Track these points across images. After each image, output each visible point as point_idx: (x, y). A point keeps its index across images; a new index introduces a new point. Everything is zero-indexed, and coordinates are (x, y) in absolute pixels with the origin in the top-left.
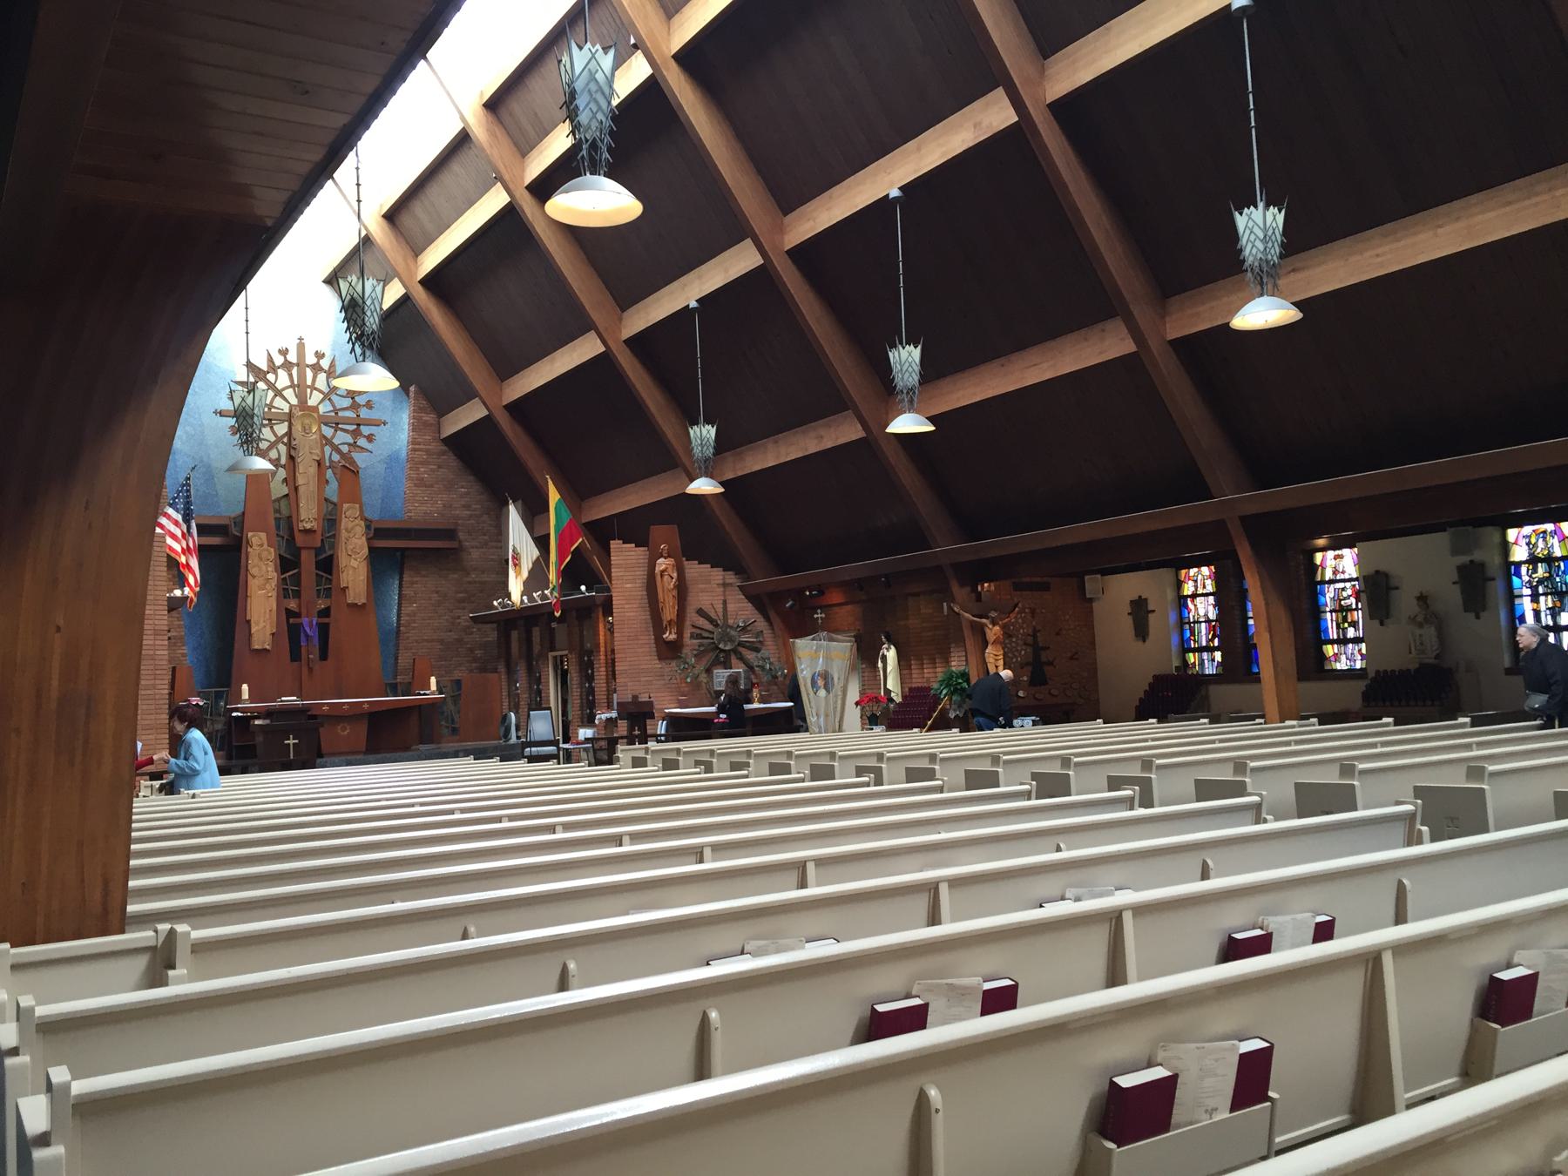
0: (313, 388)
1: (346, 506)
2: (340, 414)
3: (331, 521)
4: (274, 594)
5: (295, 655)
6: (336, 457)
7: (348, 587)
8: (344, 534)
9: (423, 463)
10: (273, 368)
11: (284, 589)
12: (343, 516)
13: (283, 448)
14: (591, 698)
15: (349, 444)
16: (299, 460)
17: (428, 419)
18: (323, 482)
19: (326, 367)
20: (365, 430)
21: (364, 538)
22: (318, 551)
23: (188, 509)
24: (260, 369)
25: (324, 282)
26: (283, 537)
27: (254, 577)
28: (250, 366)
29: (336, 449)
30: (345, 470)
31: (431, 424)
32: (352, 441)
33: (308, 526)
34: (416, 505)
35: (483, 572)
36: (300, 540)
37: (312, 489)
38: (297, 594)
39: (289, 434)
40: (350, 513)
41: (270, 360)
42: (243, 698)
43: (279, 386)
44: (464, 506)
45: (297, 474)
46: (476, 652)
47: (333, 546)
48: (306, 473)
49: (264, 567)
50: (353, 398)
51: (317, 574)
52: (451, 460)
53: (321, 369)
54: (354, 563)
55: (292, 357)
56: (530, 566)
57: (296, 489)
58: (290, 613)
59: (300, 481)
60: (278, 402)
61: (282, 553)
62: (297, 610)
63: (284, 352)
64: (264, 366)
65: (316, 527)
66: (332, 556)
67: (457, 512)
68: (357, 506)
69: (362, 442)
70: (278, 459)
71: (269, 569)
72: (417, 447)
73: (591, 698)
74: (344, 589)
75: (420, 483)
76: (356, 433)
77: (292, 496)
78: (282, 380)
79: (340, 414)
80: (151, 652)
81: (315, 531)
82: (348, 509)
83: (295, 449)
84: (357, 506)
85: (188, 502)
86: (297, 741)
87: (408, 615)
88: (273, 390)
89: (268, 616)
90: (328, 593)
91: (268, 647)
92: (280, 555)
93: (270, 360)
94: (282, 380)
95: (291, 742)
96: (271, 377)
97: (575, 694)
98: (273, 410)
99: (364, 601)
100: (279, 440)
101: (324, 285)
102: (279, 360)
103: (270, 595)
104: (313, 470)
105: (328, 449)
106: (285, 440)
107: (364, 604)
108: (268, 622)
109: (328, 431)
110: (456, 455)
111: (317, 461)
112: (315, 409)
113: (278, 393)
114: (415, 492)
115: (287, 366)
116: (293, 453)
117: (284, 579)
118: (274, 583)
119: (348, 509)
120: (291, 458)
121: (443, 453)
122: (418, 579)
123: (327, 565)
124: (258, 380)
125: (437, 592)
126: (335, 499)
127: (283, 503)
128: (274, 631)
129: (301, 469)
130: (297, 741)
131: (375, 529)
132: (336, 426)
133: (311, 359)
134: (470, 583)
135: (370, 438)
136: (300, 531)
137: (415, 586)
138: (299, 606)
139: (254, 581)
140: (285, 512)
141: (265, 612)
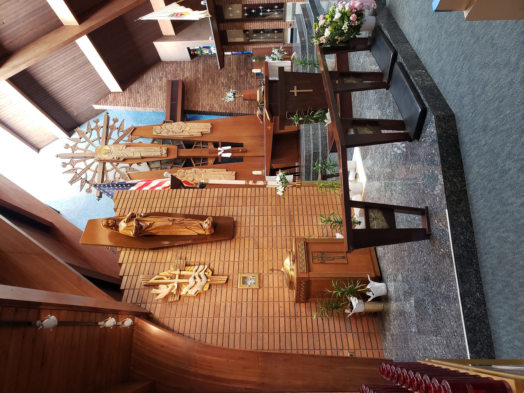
0: (86, 150)
1: (154, 133)
2: (101, 136)
3: (164, 141)
4: (204, 170)
5: (240, 159)
6: (126, 138)
7: (201, 132)
8: (170, 134)
9: (136, 101)
10: (74, 170)
11: (202, 165)
12: (160, 134)
13: (121, 165)
14: (276, 7)
15: (119, 132)
16: (126, 156)
17: (111, 98)
18: (140, 145)
19: (74, 143)
20: (111, 123)
21: (173, 124)
22: (179, 147)
23: (117, 185)
24: (74, 177)
25: (38, 152)
26: (172, 166)
27: (194, 180)
28: (72, 182)
29: (121, 138)
30: (134, 133)
31: (115, 97)
32: (117, 130)
33: (164, 152)
34: (159, 104)
35: (198, 71)
36: (173, 156)
37: (143, 150)
38: (205, 159)
39: (111, 162)
40: (156, 131)
41: (69, 171)
42: (261, 174)
43: (84, 167)
44: (160, 80)
45: (134, 157)
46: (242, 74)
47: (178, 140)
48: (131, 152)
49: (189, 175)
50: (92, 130)
51: (194, 148)
52: (134, 86)
53: (75, 146)
54: (188, 129)
55: (67, 161)
56: (183, 7)
57: (143, 158)
58: (216, 162)
59: (138, 155)
60: (93, 167)
61: (182, 166)
62: (215, 159)
63: (64, 165)
64: (71, 175)
65: (165, 148)
66: (184, 141)
67: (164, 83)
68: (154, 127)
69: (117, 125)
70: (126, 167)
71: (189, 172)
72: (126, 103)
73: (276, 7)
74: (202, 134)
75: (147, 103)
76: (113, 128)
77: (148, 160)
78: (81, 165)
79: (101, 136)
80: (215, 199)
81: (168, 148)
82: (156, 131)
83: (119, 158)
84: (154, 127)
85: (113, 186)
86: (296, 95)
87: (220, 109)
88: (86, 170)
89: (217, 173)
90: (205, 143)
91: (234, 173)
92: (183, 167)
93: (69, 171)
94: (81, 165)
95: (295, 91)
96: (79, 171)
97: (271, 46)
98: (87, 152)
99: (209, 124)
100: (114, 167)
101: (40, 153)
102: (69, 167)
103: (204, 172)
104: (132, 149)
105: (121, 142)
106: (115, 164)
107: (211, 124)
108: (220, 172)
109: (111, 142)
110: (132, 84)
111: (127, 146)
112: (97, 148)
113: (88, 167)
114: (152, 105)
115: (72, 164)
116: (122, 159)
117: (196, 165)
118: (198, 170)
119: (156, 131)
120: (125, 160)
121: (131, 90)
122: (200, 103)
123: (189, 144)
124: (80, 178)
125: (208, 94)
126: (151, 140)
127: (152, 166)
128: (225, 170)
129: (131, 155)
130: (296, 95)
131: (171, 119)
132: (107, 138)
133: (69, 151)
134: (203, 78)
135: (116, 121)
136: (167, 156)
137: (204, 105)
138: (212, 157)
139: (196, 180)
140: (158, 165)
141: (214, 174)
